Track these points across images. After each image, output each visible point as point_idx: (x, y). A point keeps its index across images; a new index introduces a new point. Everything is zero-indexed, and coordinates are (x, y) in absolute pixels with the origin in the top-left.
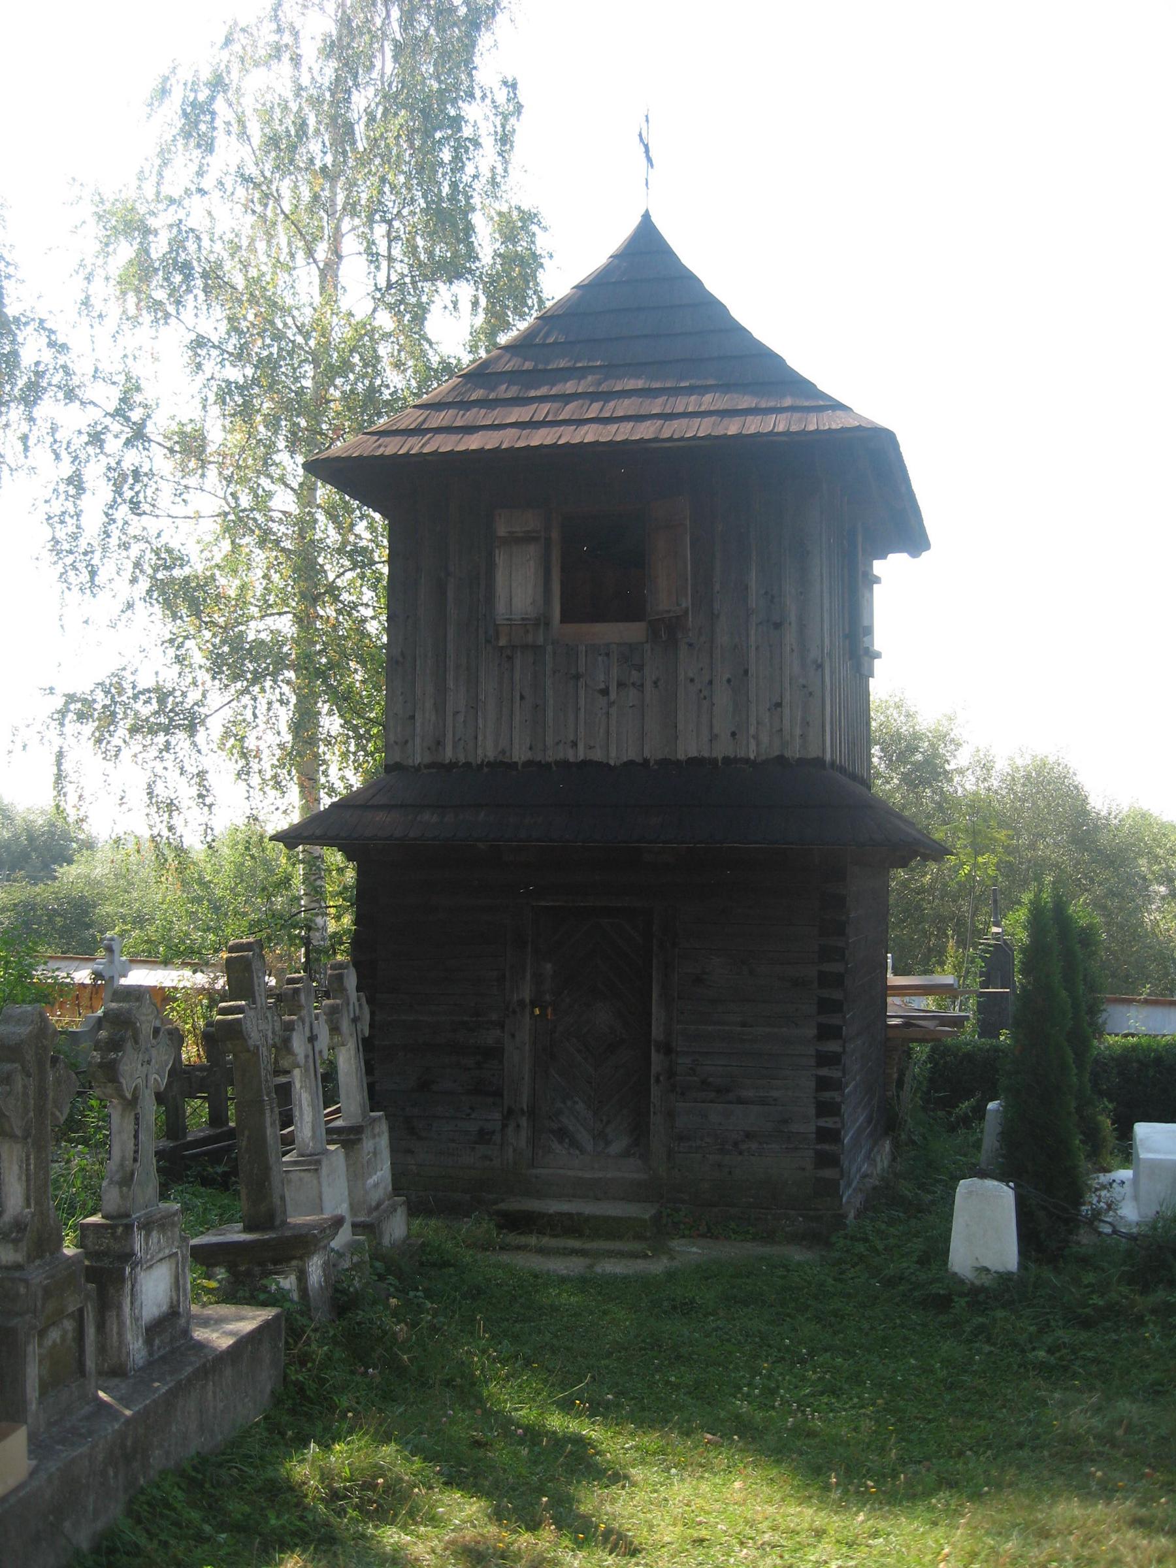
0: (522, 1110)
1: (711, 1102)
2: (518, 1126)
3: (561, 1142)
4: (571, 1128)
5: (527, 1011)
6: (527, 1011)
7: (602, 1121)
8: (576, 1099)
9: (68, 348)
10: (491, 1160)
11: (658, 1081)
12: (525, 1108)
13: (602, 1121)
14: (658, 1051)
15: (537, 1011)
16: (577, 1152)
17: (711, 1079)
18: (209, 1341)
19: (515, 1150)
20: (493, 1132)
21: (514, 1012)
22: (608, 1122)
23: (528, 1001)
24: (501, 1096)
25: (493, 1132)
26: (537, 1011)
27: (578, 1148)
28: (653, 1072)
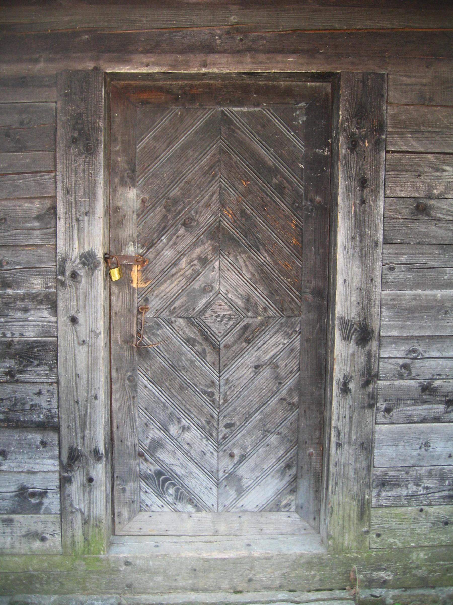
0: (96, 452)
1: (437, 420)
2: (90, 480)
3: (161, 494)
4: (178, 470)
5: (100, 274)
6: (100, 274)
7: (232, 456)
8: (185, 422)
9: (77, 323)
10: (43, 539)
11: (345, 390)
12: (102, 449)
13: (232, 456)
14: (346, 338)
15: (115, 274)
16: (189, 508)
17: (437, 383)
18: (98, 200)
19: (86, 522)
20: (44, 494)
21: (74, 275)
22: (243, 457)
23: (100, 255)
24: (57, 429)
25: (44, 494)
26: (115, 274)
27: (190, 501)
28: (338, 375)
